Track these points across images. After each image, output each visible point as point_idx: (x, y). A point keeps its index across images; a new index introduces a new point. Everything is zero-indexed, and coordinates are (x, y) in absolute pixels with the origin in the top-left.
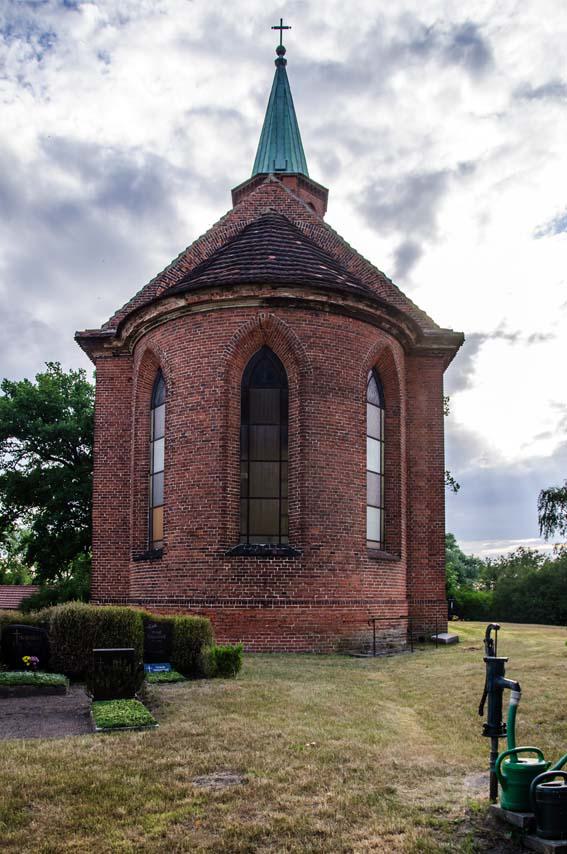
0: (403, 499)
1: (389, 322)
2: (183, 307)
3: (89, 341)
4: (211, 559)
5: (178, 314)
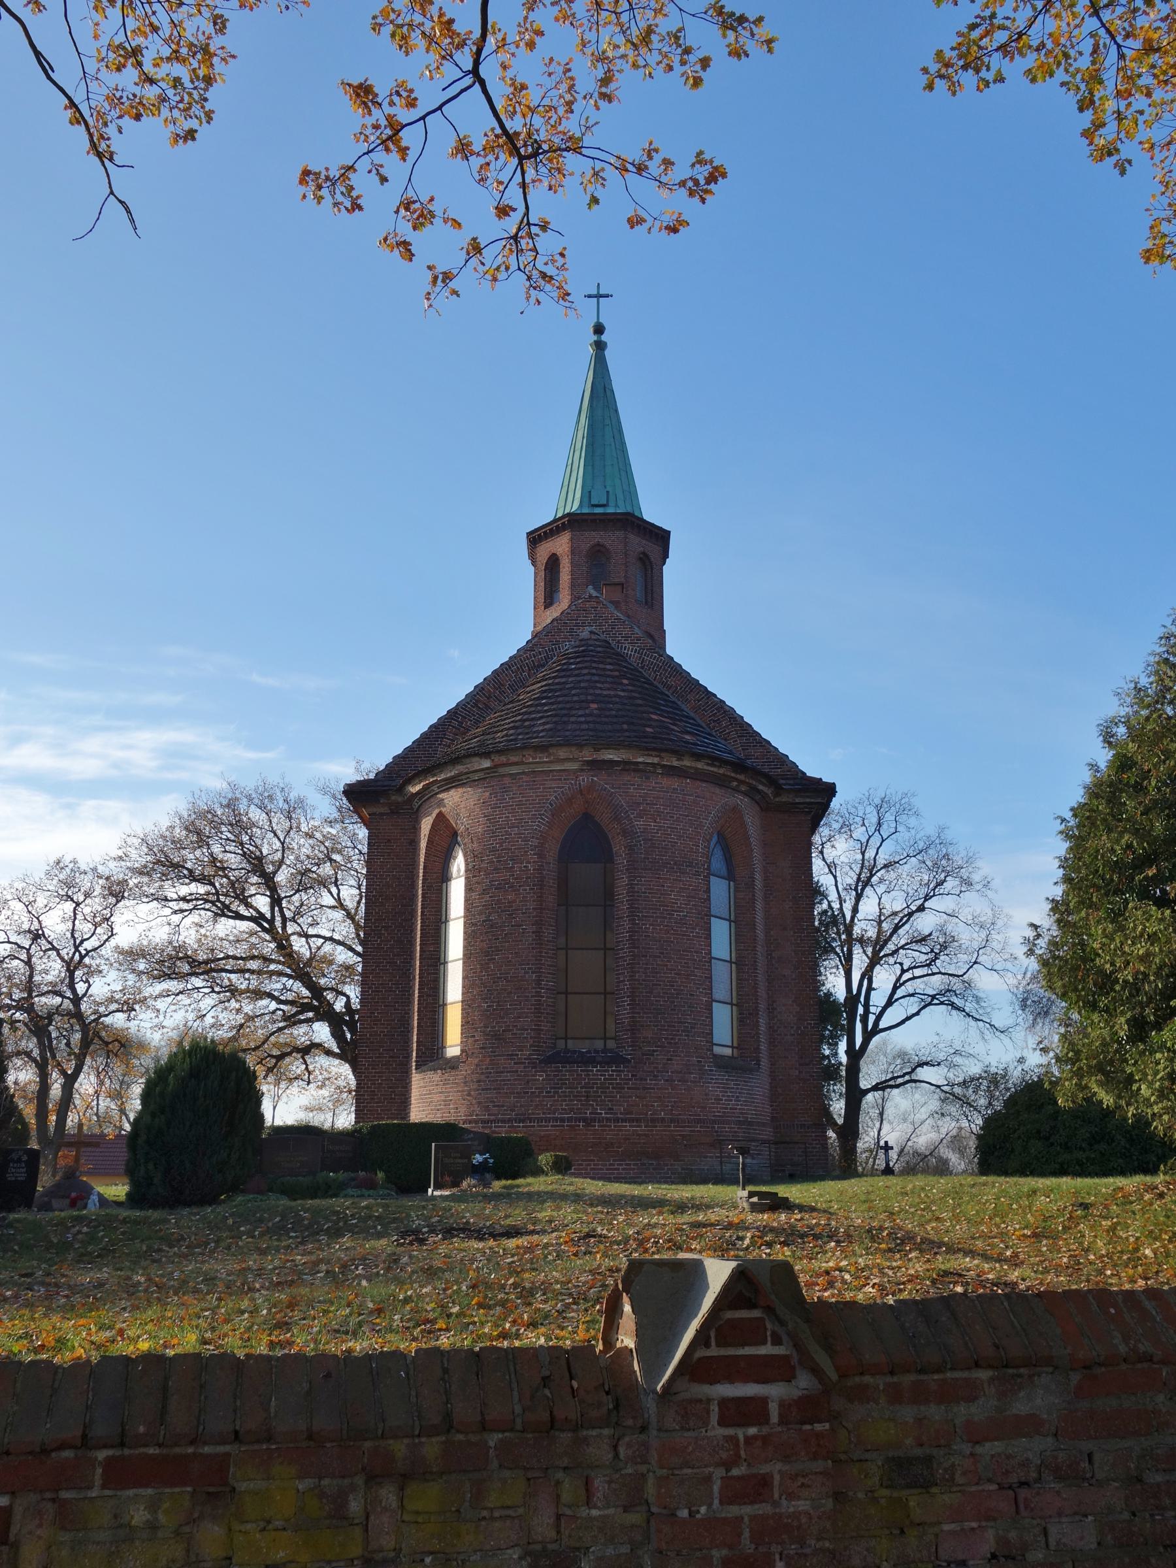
0: (762, 992)
1: (736, 780)
2: (487, 768)
3: (886, 1142)
4: (521, 1068)
5: (481, 775)
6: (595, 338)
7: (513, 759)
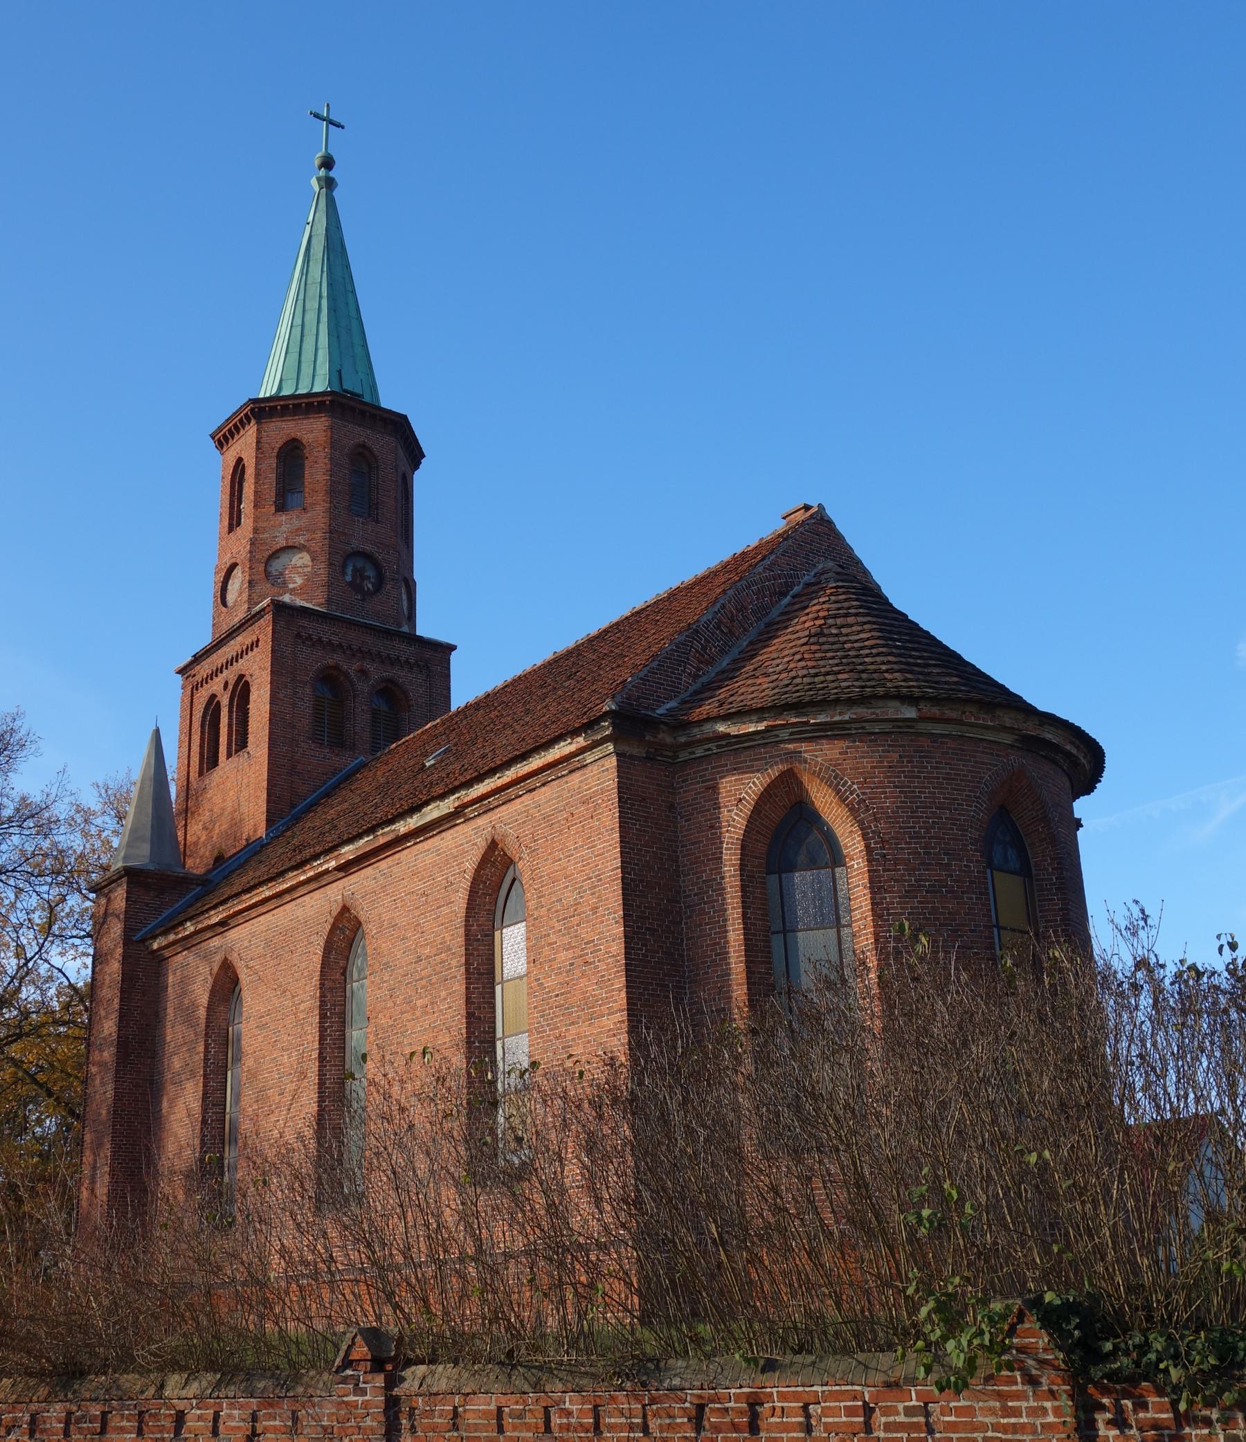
5: (887, 727)
6: (332, 174)
7: (949, 713)
